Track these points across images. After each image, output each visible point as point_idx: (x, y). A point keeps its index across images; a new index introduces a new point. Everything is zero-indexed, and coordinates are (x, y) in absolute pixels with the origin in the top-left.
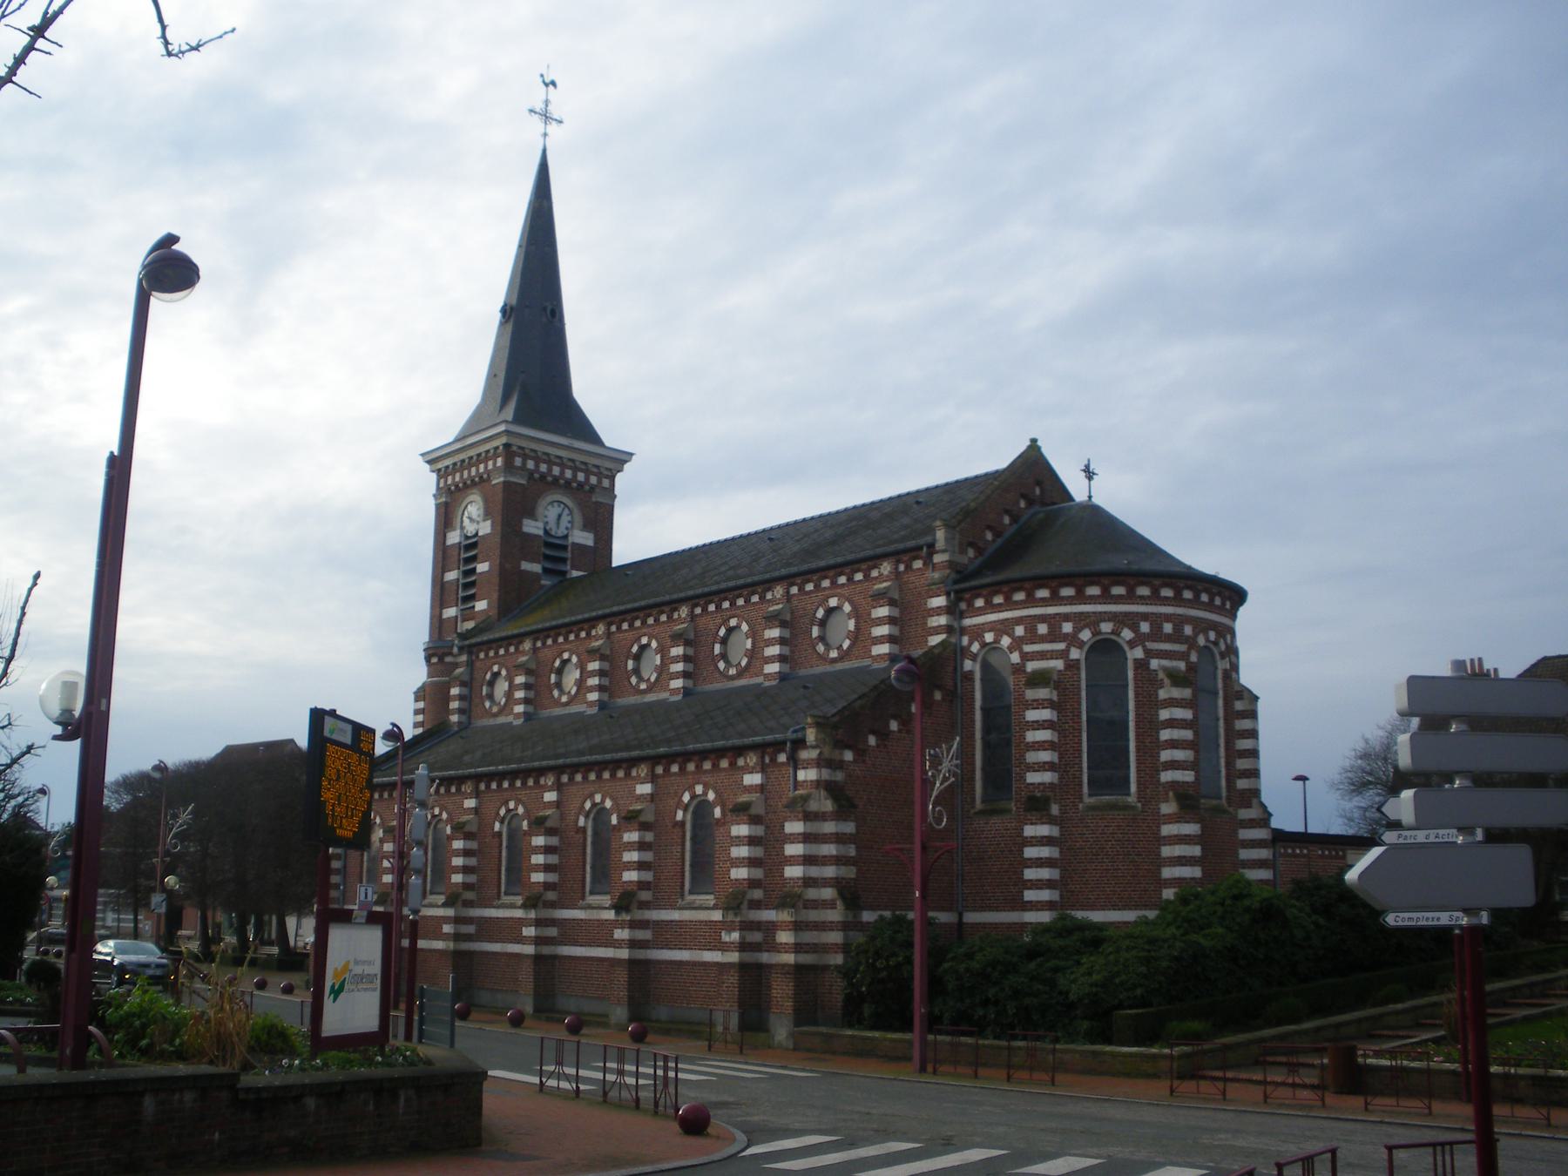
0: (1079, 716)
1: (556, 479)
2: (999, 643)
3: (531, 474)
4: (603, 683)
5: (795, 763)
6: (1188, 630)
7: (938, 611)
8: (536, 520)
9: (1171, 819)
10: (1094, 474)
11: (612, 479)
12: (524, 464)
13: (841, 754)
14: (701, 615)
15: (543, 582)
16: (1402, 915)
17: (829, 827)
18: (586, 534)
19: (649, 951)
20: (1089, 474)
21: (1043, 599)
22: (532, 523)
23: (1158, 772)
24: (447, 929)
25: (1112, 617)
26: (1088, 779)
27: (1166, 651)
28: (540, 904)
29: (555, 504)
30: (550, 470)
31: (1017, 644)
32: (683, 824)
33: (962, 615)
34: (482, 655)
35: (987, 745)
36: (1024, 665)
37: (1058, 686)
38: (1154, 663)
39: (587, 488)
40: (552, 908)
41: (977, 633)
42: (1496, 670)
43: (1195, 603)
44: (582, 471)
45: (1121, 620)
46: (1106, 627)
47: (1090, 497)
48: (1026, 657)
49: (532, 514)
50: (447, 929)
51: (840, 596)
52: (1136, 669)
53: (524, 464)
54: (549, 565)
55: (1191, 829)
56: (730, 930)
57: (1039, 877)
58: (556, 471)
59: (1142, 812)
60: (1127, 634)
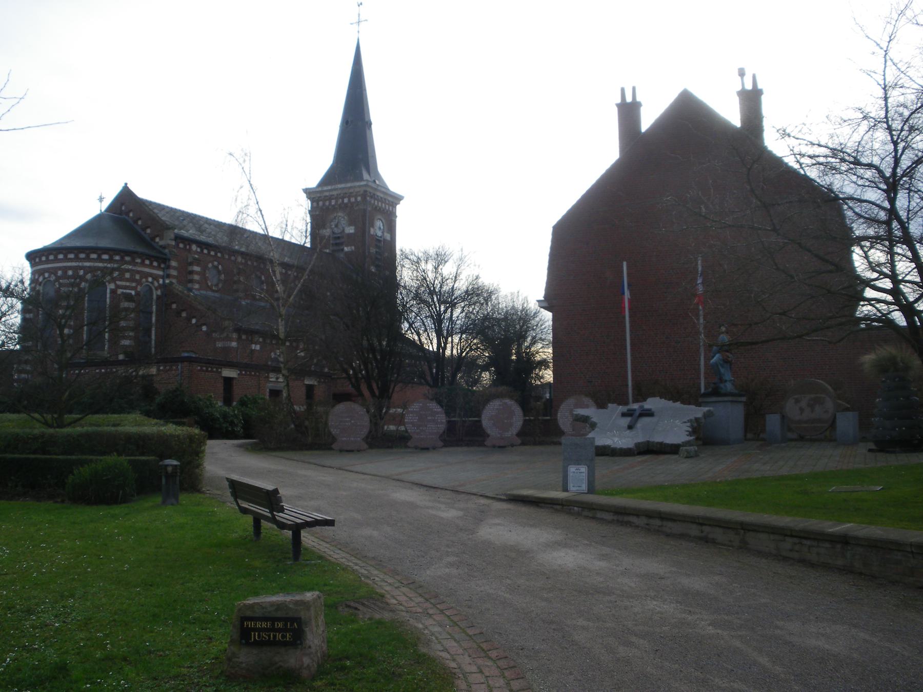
6: (137, 277)
36: (116, 291)
52: (111, 293)
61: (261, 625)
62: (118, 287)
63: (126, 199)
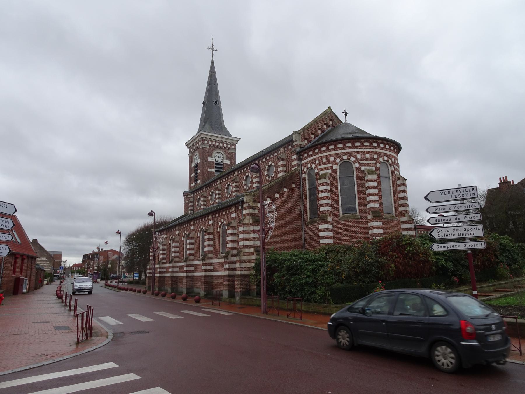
0: (337, 188)
1: (218, 147)
2: (312, 167)
3: (210, 145)
4: (219, 197)
5: (243, 209)
6: (376, 156)
7: (294, 160)
8: (212, 157)
9: (372, 220)
10: (347, 114)
11: (235, 145)
12: (208, 142)
13: (257, 205)
14: (240, 174)
15: (215, 174)
16: (440, 245)
17: (251, 228)
18: (227, 161)
19: (212, 272)
20: (345, 113)
21: (324, 151)
22: (211, 158)
23: (366, 205)
24: (185, 269)
25: (347, 154)
26: (342, 209)
27: (367, 164)
28: (188, 260)
29: (218, 153)
30: (216, 144)
31: (316, 167)
32: (219, 232)
33: (301, 160)
34: (196, 194)
35: (311, 201)
37: (329, 178)
38: (363, 168)
39: (227, 148)
40: (192, 261)
41: (305, 165)
42: (513, 181)
43: (378, 147)
44: (225, 144)
45: (350, 154)
46: (345, 157)
47: (346, 121)
48: (319, 170)
49: (211, 156)
50: (185, 269)
51: (271, 161)
52: (356, 170)
53: (208, 142)
54: (217, 169)
55: (379, 223)
56: (226, 264)
57: (325, 242)
58: (218, 144)
59: (361, 219)
60: (353, 159)
61: (143, 276)
62: (361, 165)
63: (37, 240)
